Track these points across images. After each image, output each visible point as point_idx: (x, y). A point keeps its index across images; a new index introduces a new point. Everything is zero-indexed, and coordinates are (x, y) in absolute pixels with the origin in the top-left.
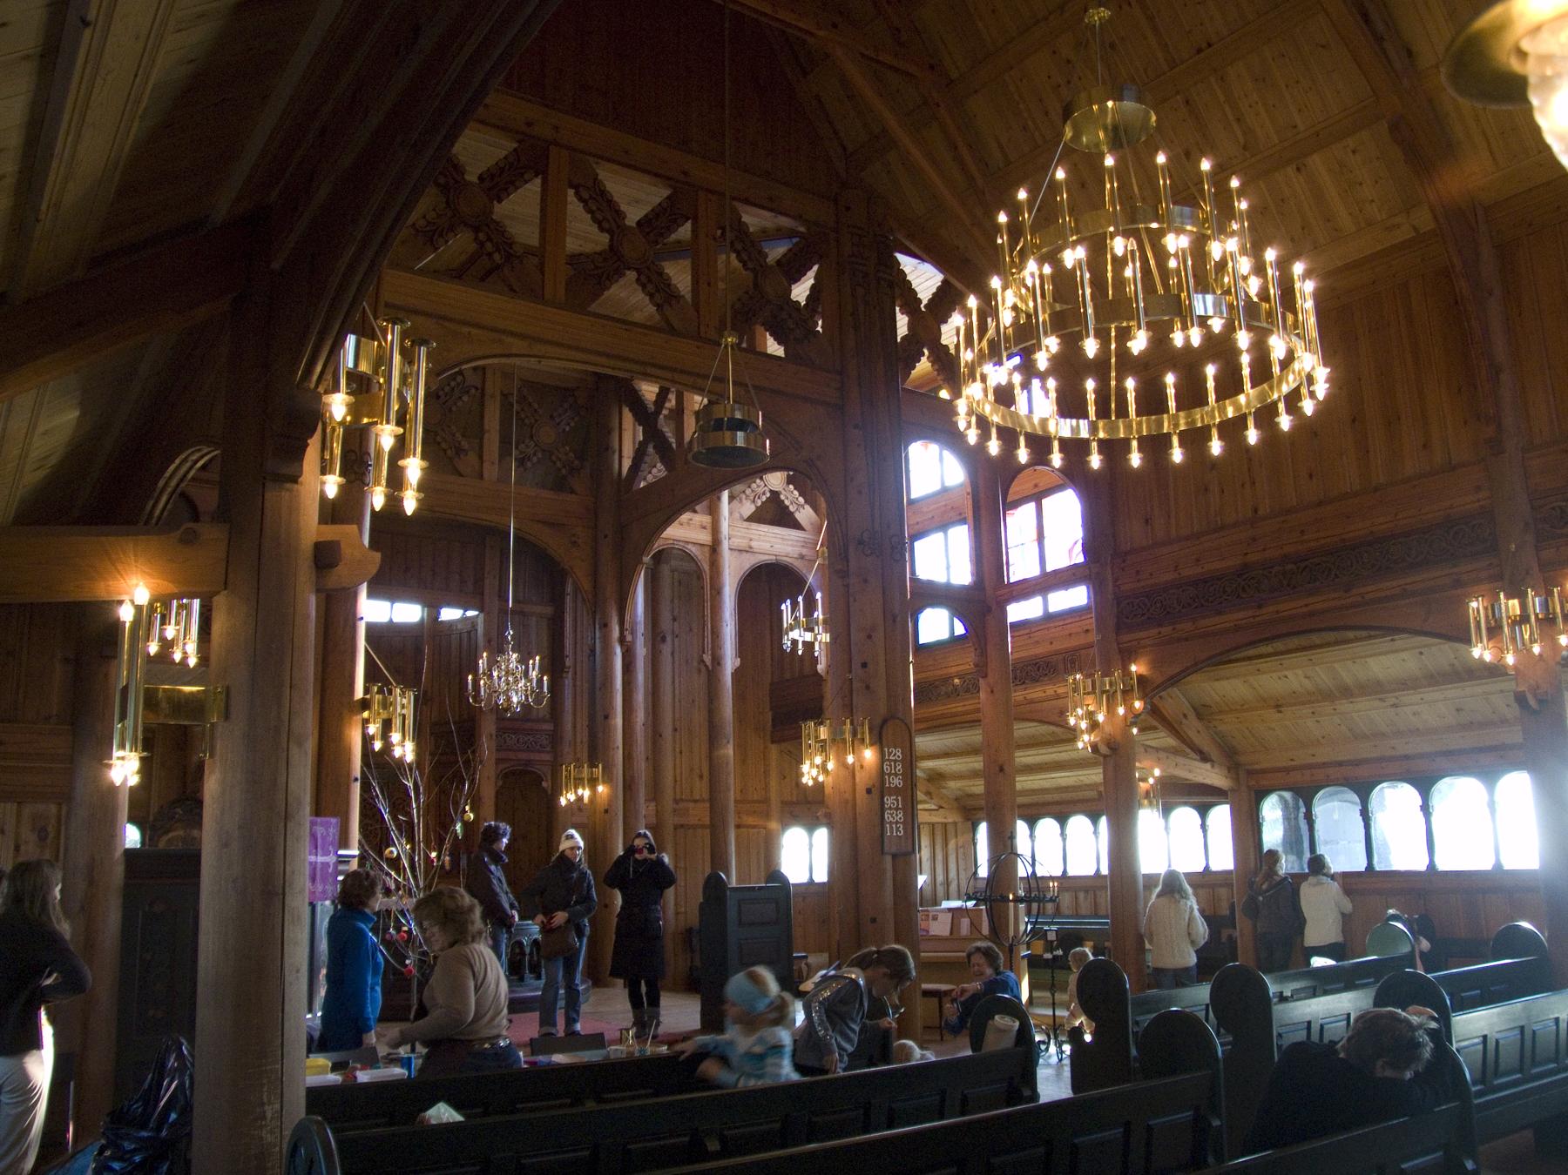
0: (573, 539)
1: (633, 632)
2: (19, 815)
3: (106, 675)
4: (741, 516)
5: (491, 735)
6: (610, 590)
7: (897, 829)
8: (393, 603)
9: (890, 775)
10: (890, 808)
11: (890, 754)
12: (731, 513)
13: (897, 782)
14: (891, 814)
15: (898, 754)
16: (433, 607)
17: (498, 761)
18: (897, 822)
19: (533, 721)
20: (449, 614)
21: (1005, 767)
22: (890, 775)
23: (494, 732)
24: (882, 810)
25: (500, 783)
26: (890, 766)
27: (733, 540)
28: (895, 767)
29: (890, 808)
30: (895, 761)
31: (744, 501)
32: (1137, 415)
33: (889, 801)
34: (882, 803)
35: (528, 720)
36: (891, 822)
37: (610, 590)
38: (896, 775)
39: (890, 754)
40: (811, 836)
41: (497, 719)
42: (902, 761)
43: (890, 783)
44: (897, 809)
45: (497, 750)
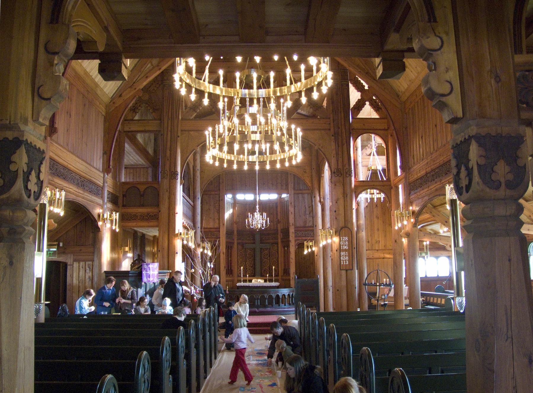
0: (305, 170)
1: (324, 199)
2: (85, 264)
3: (98, 235)
4: (366, 154)
5: (293, 232)
6: (316, 186)
7: (346, 262)
8: (245, 199)
9: (343, 245)
10: (343, 256)
11: (343, 239)
12: (362, 154)
13: (346, 247)
14: (343, 258)
15: (347, 239)
16: (280, 194)
17: (295, 241)
18: (346, 260)
19: (307, 227)
20: (284, 196)
21: (397, 241)
22: (343, 245)
23: (294, 231)
24: (340, 256)
25: (297, 247)
26: (343, 243)
27: (363, 163)
28: (345, 243)
29: (343, 256)
30: (345, 241)
31: (367, 149)
32: (269, 154)
33: (342, 253)
34: (340, 254)
35: (305, 227)
36: (343, 260)
37: (316, 186)
38: (345, 245)
39: (343, 239)
40: (437, 260)
41: (295, 227)
42: (348, 241)
43: (343, 248)
44: (346, 256)
45: (295, 237)
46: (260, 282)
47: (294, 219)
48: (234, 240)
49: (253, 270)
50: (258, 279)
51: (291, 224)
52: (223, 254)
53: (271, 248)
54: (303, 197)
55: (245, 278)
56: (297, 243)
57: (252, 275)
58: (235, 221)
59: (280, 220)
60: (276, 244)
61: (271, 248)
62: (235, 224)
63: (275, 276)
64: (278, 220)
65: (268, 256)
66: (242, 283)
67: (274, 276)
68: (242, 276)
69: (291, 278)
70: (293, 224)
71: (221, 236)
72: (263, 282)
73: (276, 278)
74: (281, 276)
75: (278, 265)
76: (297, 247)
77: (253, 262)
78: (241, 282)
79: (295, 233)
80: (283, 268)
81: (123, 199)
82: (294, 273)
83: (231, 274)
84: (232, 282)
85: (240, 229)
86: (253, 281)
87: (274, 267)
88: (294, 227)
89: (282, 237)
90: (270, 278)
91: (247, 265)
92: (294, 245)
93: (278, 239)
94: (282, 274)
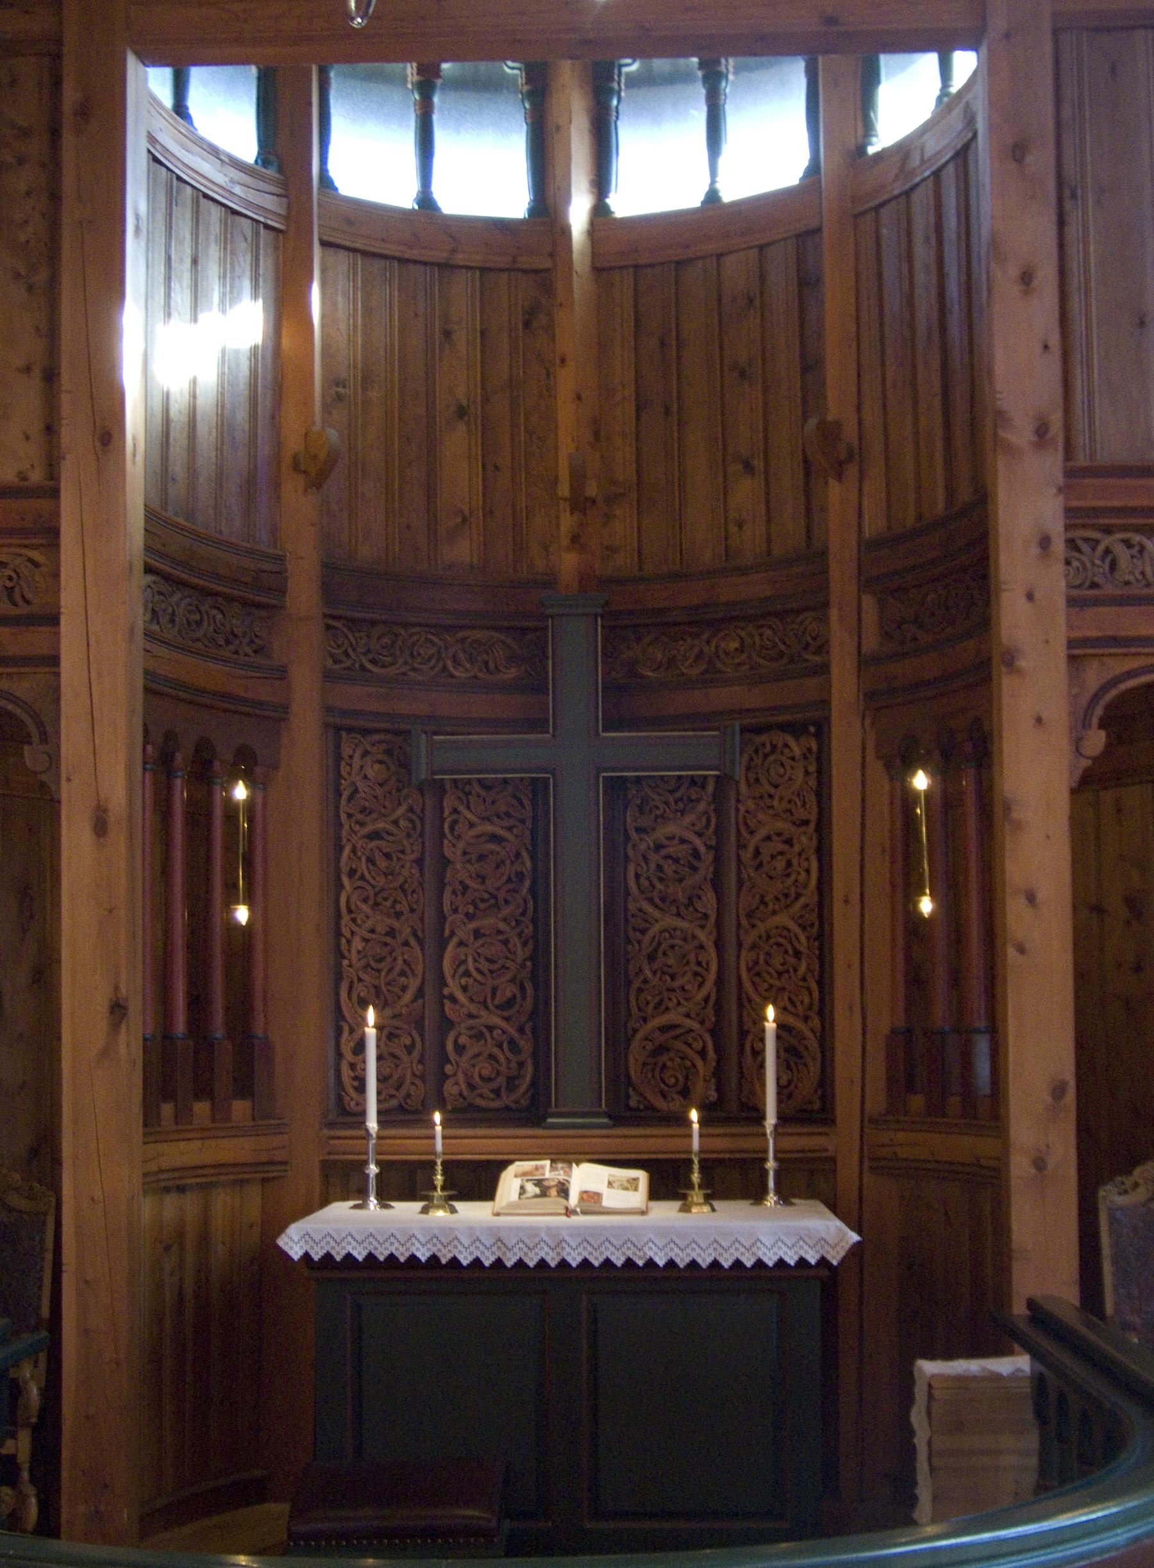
5: (1045, 542)
23: (1056, 527)
41: (1070, 473)
46: (591, 1199)
47: (1054, 361)
48: (282, 674)
49: (526, 1045)
50: (568, 1156)
51: (1020, 434)
52: (100, 827)
53: (739, 773)
54: (1000, 399)
55: (407, 1145)
56: (1093, 677)
57: (507, 1100)
58: (293, 443)
59: (850, 433)
60: (795, 729)
61: (739, 773)
62: (293, 488)
63: (782, 1118)
64: (830, 432)
65: (706, 868)
66: (373, 1201)
67: (771, 1120)
68: (372, 1124)
69: (1020, 1167)
70: (1042, 431)
71: (69, 600)
72: (638, 1198)
73: (805, 1141)
74: (867, 1121)
75: (824, 982)
76: (1097, 740)
77: (521, 953)
78: (362, 1193)
79: (1071, 543)
80: (883, 1022)
81: (144, 777)
82: (1058, 1091)
83: (244, 1087)
84: (254, 1193)
85: (366, 552)
86: (510, 1184)
87: (770, 1012)
88: (1051, 464)
89: (871, 643)
90: (726, 1143)
91: (453, 987)
92: (1057, 711)
93: (823, 669)
94: (877, 1101)
